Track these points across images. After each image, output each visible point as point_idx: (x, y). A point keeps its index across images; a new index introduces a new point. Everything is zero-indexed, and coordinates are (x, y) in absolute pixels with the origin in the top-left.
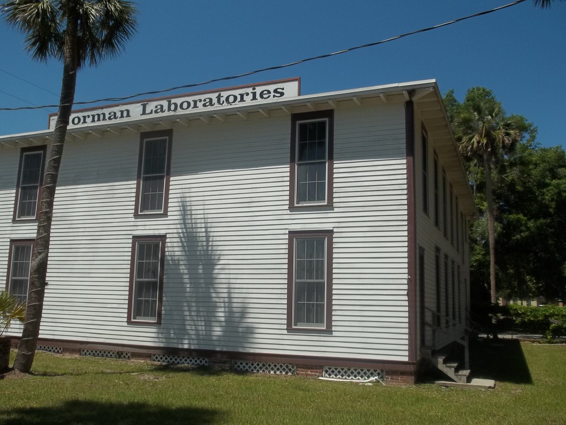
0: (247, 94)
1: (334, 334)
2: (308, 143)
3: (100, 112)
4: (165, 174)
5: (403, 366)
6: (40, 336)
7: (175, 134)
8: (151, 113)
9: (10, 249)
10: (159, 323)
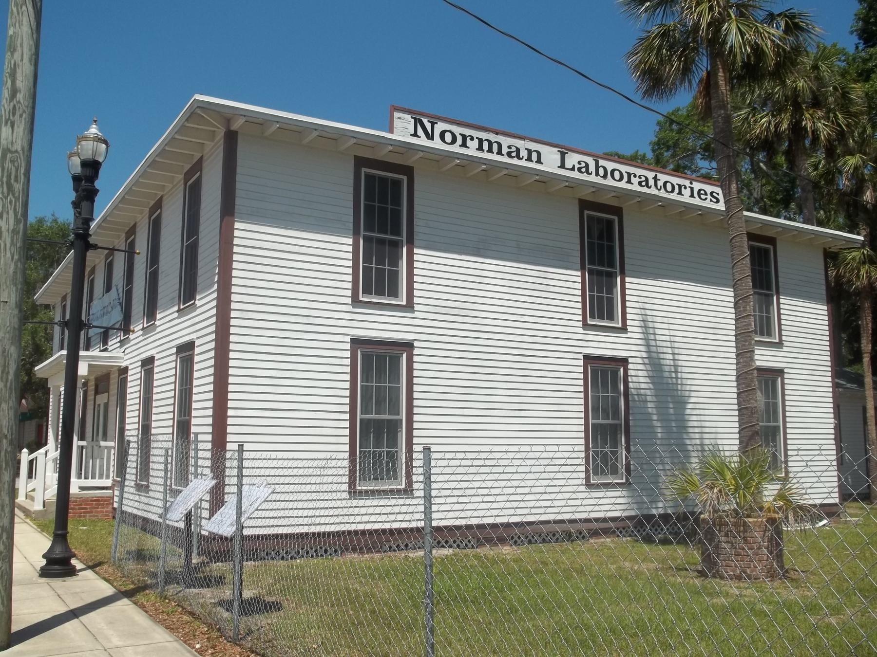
0: (472, 139)
3: (492, 137)
8: (573, 169)
9: (585, 372)
10: (626, 485)
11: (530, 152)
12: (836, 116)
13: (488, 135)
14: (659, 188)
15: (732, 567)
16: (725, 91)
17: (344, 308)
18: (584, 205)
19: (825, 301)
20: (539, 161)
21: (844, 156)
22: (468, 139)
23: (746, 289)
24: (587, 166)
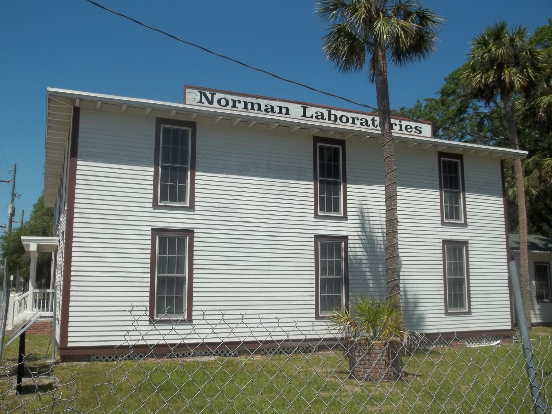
0: (240, 102)
1: (473, 314)
2: (324, 162)
3: (254, 100)
4: (189, 166)
5: (509, 332)
6: (69, 345)
7: (464, 157)
8: (312, 117)
11: (281, 108)
12: (527, 71)
13: (251, 99)
14: (376, 126)
15: (361, 372)
16: (382, 64)
17: (147, 210)
18: (317, 139)
19: (502, 195)
20: (287, 113)
21: (541, 96)
22: (356, 119)
23: (392, 192)
24: (322, 114)
